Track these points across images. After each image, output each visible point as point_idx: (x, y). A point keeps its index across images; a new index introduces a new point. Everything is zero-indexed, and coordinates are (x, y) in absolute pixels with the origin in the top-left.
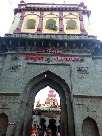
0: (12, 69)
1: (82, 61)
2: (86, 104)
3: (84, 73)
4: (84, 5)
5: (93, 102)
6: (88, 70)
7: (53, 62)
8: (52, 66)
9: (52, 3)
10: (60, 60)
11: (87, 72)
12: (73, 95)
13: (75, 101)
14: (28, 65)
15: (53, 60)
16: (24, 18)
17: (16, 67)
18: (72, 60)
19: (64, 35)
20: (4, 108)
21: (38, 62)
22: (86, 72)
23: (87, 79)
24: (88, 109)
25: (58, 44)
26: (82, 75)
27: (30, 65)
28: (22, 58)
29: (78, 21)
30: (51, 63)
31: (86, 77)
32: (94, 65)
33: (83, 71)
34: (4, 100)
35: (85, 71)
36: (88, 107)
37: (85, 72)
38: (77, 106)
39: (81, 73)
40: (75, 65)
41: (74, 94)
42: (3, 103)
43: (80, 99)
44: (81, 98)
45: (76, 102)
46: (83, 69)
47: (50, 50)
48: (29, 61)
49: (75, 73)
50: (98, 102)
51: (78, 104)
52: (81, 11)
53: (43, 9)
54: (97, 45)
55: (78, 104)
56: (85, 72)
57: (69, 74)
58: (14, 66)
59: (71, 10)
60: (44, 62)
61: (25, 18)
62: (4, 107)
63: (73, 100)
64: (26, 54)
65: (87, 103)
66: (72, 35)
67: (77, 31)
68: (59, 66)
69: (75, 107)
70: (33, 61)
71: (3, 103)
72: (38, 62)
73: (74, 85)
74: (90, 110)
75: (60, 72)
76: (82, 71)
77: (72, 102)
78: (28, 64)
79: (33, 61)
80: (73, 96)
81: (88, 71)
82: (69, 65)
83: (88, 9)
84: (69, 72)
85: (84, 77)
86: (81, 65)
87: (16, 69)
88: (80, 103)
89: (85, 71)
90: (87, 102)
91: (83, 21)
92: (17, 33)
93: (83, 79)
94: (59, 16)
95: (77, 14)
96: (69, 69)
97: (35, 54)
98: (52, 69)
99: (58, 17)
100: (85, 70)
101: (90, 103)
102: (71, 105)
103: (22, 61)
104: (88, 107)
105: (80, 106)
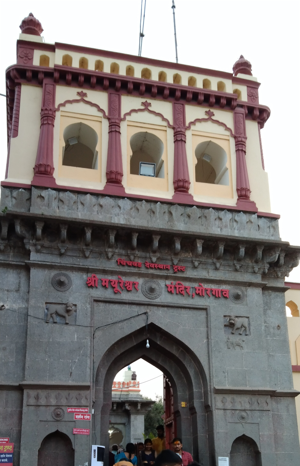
0: (54, 316)
1: (237, 297)
2: (239, 407)
3: (240, 334)
4: (249, 73)
5: (256, 403)
6: (249, 324)
7: (165, 298)
8: (160, 312)
9: (174, 35)
10: (148, 267)
11: (248, 329)
12: (212, 387)
13: (217, 402)
14: (95, 304)
15: (164, 291)
16: (53, 118)
17: (68, 311)
18: (213, 295)
19: (191, 206)
20: (58, 421)
21: (125, 296)
22: (245, 330)
23: (245, 350)
24: (243, 418)
25: (178, 246)
26: (235, 339)
27: (101, 304)
28: (77, 280)
29: (229, 147)
30: (158, 301)
31: (243, 344)
32: (265, 311)
33: (238, 329)
34: (53, 402)
35: (243, 329)
36: (244, 414)
37: (244, 330)
38: (222, 412)
39: (233, 333)
40: (219, 309)
41: (217, 387)
42: (53, 408)
43: (229, 398)
44: (230, 395)
45: (219, 405)
46: (238, 322)
47: (154, 259)
48: (99, 293)
49: (220, 334)
50: (265, 405)
51: (224, 409)
52: (242, 106)
53: (82, 79)
54: (278, 255)
55: (224, 409)
56: (244, 330)
57: (204, 335)
58: (60, 309)
59: (181, 92)
60: (139, 297)
61: (58, 114)
62: (58, 417)
63: (213, 400)
64: (87, 270)
65: (242, 406)
66: (214, 208)
67: (220, 194)
68: (179, 311)
69: (217, 415)
70: (108, 294)
71: (53, 408)
72: (125, 296)
73: (215, 363)
74: (248, 422)
75: (181, 326)
76: (235, 327)
77: (210, 404)
78: (96, 301)
79: (108, 294)
80: (212, 391)
81: (249, 327)
82: (206, 309)
83: (263, 101)
84: (203, 329)
85: (238, 345)
86: (235, 309)
87: (66, 315)
88: (229, 406)
89: (243, 329)
90: (243, 402)
91: (245, 152)
92: (46, 188)
93: (238, 348)
94: (171, 123)
95: (225, 116)
96: (205, 320)
97: (112, 273)
98: (162, 319)
99: (169, 126)
100: (243, 326)
101: (248, 406)
102: (207, 408)
103: (78, 292)
104: (244, 414)
105: (228, 412)
